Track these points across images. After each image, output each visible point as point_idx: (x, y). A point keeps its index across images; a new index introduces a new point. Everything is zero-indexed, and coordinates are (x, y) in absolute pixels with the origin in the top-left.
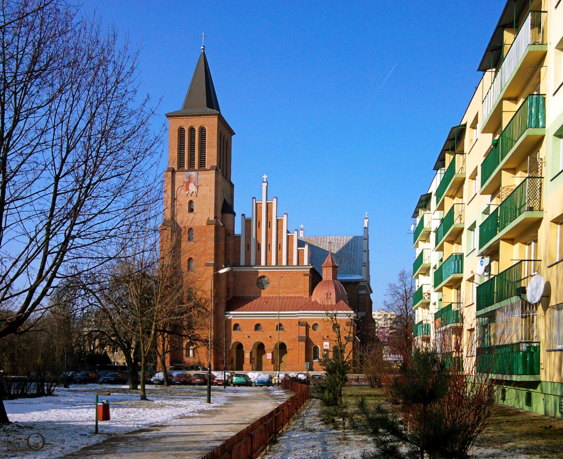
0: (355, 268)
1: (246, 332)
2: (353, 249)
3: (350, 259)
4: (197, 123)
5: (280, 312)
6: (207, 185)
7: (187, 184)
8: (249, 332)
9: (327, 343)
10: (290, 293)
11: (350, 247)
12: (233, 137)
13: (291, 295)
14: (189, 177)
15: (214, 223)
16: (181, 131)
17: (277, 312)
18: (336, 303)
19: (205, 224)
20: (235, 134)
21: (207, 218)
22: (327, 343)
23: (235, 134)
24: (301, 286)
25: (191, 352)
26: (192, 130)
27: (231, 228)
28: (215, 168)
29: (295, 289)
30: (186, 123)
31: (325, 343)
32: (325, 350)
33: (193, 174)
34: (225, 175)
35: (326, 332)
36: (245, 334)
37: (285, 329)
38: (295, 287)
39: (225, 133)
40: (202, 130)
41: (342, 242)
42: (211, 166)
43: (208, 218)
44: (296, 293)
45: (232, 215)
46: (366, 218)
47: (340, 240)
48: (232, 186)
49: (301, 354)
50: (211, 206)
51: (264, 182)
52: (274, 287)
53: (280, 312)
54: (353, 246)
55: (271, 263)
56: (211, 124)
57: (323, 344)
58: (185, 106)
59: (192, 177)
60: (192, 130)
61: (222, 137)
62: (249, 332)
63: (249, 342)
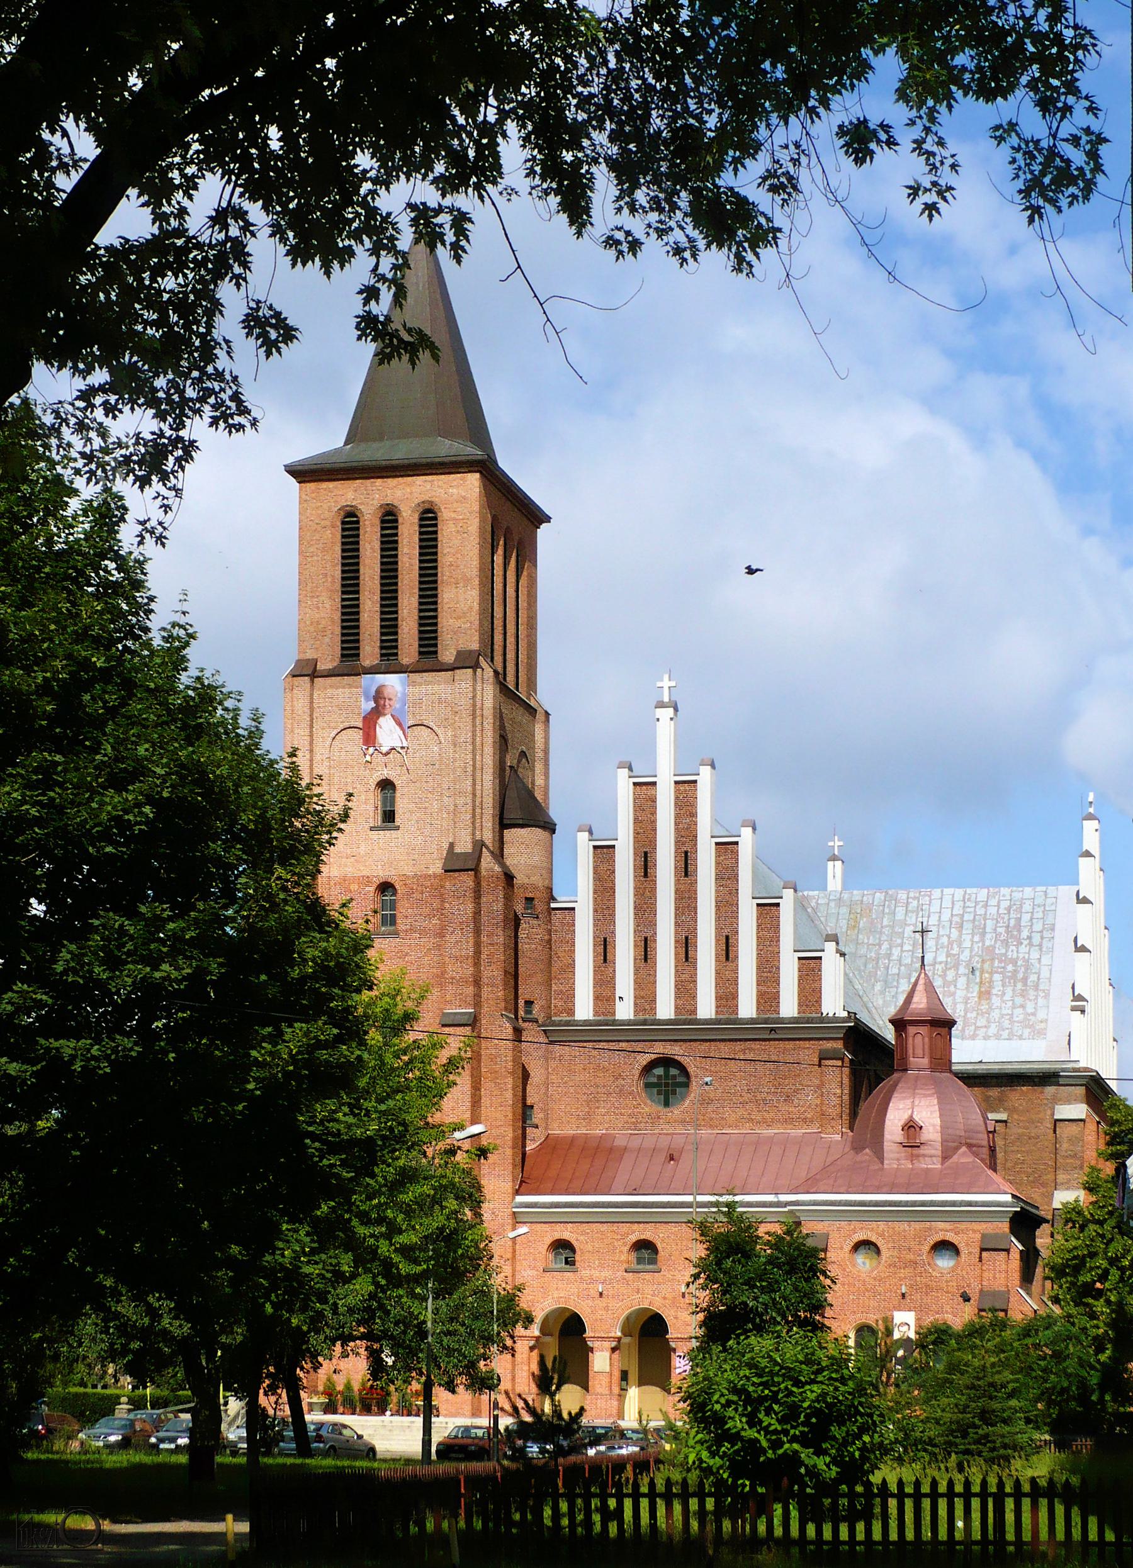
0: (1041, 1015)
1: (596, 1274)
2: (1036, 939)
3: (1025, 980)
4: (408, 494)
7: (370, 723)
11: (1025, 933)
12: (543, 532)
14: (379, 696)
16: (350, 522)
17: (689, 1199)
18: (945, 1158)
19: (437, 868)
20: (548, 519)
21: (446, 846)
23: (548, 519)
26: (389, 518)
27: (466, 1017)
29: (784, 1108)
30: (368, 497)
33: (393, 682)
35: (903, 1273)
36: (592, 1281)
38: (788, 1099)
39: (514, 520)
40: (429, 518)
41: (993, 910)
42: (459, 653)
43: (452, 845)
44: (789, 1121)
45: (537, 834)
46: (1090, 817)
47: (986, 906)
51: (661, 705)
53: (700, 1198)
54: (1038, 927)
56: (460, 498)
59: (387, 692)
60: (389, 518)
63: (607, 1308)
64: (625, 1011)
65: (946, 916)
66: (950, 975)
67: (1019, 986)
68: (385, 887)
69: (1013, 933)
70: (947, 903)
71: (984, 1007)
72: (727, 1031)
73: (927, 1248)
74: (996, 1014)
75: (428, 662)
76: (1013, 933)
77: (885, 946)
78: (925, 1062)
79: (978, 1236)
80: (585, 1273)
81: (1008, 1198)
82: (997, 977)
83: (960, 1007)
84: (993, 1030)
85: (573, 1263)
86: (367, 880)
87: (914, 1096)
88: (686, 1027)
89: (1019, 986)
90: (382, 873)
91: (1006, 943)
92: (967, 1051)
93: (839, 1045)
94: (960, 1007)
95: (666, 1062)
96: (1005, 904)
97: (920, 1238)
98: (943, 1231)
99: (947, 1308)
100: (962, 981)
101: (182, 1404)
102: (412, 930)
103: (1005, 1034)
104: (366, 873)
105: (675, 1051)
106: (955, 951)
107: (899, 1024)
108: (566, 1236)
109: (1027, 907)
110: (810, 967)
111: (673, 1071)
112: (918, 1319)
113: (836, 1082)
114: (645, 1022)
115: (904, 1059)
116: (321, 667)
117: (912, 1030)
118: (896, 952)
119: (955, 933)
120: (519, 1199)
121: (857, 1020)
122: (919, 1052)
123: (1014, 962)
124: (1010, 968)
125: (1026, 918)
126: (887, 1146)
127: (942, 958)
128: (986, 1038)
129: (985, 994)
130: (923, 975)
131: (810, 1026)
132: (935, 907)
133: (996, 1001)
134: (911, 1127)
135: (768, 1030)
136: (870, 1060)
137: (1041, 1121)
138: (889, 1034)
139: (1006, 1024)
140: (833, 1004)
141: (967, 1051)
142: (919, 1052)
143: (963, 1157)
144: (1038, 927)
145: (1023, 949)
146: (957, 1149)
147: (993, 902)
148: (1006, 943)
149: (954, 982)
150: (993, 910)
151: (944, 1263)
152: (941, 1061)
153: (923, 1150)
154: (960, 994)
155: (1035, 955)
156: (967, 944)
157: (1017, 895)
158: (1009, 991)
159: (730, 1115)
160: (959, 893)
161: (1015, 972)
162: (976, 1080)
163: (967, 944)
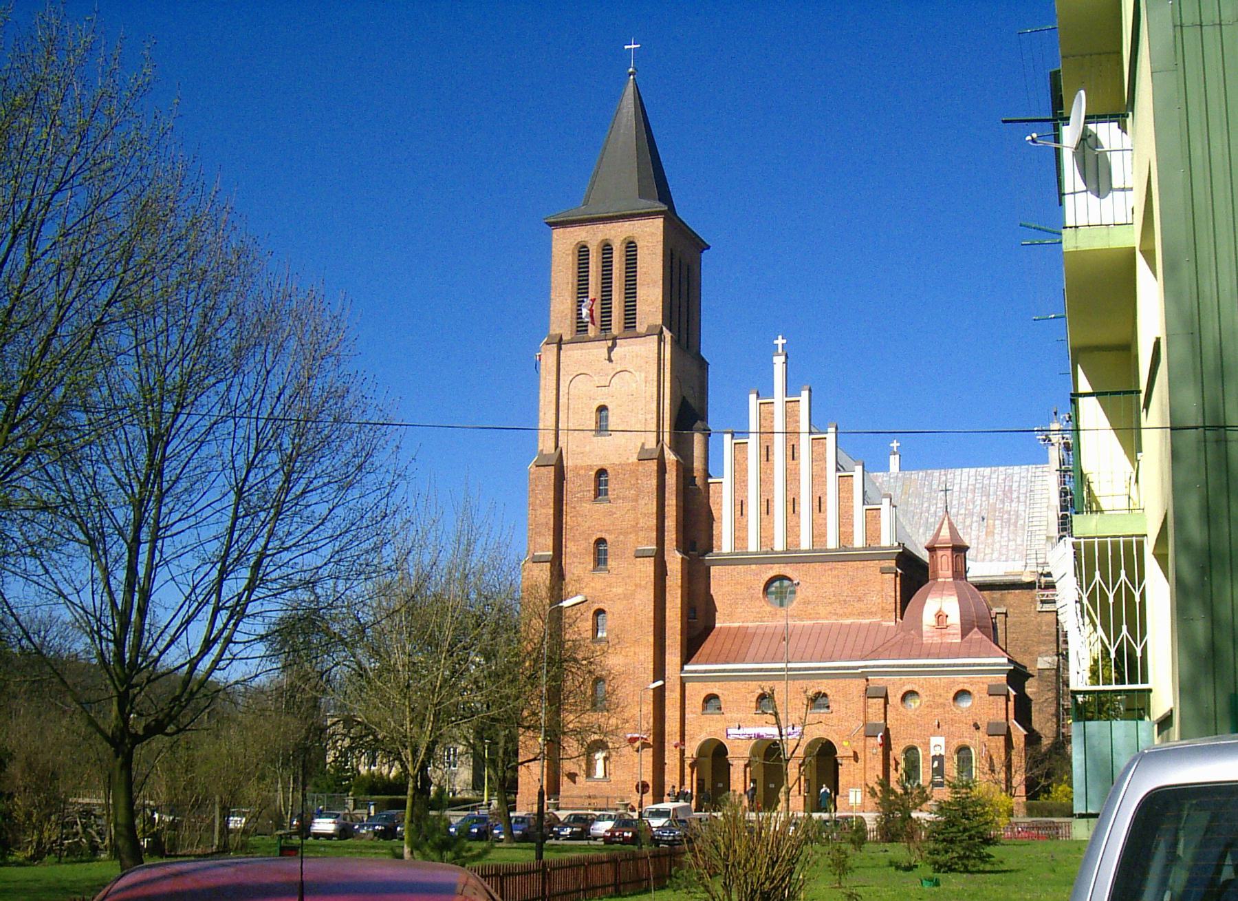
2: (1022, 498)
4: (617, 233)
5: (790, 665)
6: (639, 369)
8: (741, 715)
9: (941, 740)
10: (847, 616)
11: (1015, 495)
13: (848, 622)
15: (656, 455)
17: (783, 665)
18: (963, 636)
19: (634, 459)
20: (708, 247)
22: (941, 740)
24: (876, 599)
25: (600, 765)
26: (607, 248)
28: (658, 331)
31: (934, 741)
32: (935, 758)
34: (684, 341)
37: (833, 706)
38: (860, 600)
40: (631, 247)
43: (643, 444)
44: (861, 614)
48: (703, 365)
49: (873, 768)
50: (649, 416)
52: (806, 602)
53: (790, 665)
54: (1023, 490)
55: (799, 545)
56: (649, 235)
57: (928, 743)
58: (122, 869)
60: (607, 248)
61: (676, 260)
62: (741, 715)
64: (753, 546)
65: (964, 486)
66: (968, 522)
67: (1012, 528)
68: (601, 472)
69: (1007, 494)
70: (965, 476)
71: (990, 541)
72: (818, 557)
73: (951, 701)
74: (997, 546)
75: (629, 333)
76: (1007, 494)
77: (926, 505)
78: (950, 573)
79: (986, 686)
80: (728, 715)
81: (1005, 660)
82: (997, 522)
83: (974, 541)
84: (996, 555)
85: (720, 708)
86: (590, 468)
87: (942, 595)
88: (793, 556)
89: (1012, 528)
90: (599, 463)
91: (1003, 502)
92: (978, 569)
93: (893, 563)
94: (974, 541)
95: (782, 578)
96: (1002, 477)
97: (947, 688)
98: (962, 682)
99: (966, 734)
100: (975, 525)
101: (928, 656)
102: (618, 498)
103: (1004, 558)
104: (589, 463)
105: (786, 570)
106: (971, 507)
107: (931, 549)
108: (715, 691)
109: (1016, 478)
110: (872, 515)
111: (786, 583)
112: (947, 742)
113: (887, 587)
114: (767, 553)
115: (935, 572)
116: (564, 338)
117: (940, 553)
118: (933, 509)
119: (970, 496)
120: (686, 668)
121: (904, 549)
122: (945, 567)
123: (1009, 513)
124: (1006, 516)
125: (1015, 486)
126: (925, 628)
127: (962, 511)
128: (991, 561)
129: (990, 533)
130: (946, 522)
131: (870, 554)
132: (957, 481)
133: (997, 537)
134: (940, 616)
135: (844, 555)
136: (912, 574)
137: (1029, 613)
138: (925, 556)
139: (1004, 551)
140: (886, 540)
141: (978, 569)
142: (945, 567)
143: (976, 634)
144: (1023, 490)
145: (1014, 505)
146: (972, 629)
147: (994, 476)
148: (1003, 502)
149: (970, 527)
150: (994, 481)
151: (965, 704)
152: (960, 573)
153: (949, 630)
154: (974, 533)
155: (1022, 508)
156: (978, 502)
157: (1010, 471)
158: (1005, 531)
159: (822, 610)
160: (973, 471)
161: (1009, 519)
162: (982, 587)
163: (978, 502)
